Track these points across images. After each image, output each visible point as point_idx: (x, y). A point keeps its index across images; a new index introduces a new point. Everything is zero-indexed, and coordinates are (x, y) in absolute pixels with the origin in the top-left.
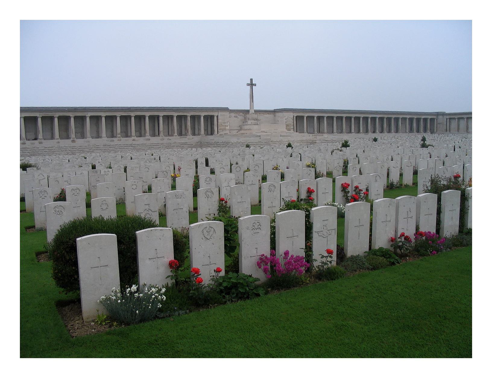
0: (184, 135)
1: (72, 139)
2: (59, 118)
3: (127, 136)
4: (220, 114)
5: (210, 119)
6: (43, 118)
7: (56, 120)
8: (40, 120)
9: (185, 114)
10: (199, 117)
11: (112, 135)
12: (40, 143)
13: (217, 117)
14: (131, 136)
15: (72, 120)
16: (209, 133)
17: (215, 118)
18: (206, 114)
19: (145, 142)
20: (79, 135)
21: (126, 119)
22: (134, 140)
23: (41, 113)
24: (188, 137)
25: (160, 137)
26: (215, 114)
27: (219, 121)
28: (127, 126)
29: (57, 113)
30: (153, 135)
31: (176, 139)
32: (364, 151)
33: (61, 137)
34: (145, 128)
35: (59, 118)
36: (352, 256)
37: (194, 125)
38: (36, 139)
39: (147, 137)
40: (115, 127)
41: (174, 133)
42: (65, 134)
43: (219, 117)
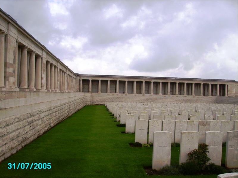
0: (206, 95)
1: (143, 94)
2: (137, 82)
3: (173, 94)
4: (229, 84)
5: (223, 87)
6: (128, 82)
7: (135, 83)
8: (127, 83)
9: (208, 83)
10: (116, 81)
11: (165, 93)
12: (126, 95)
13: (228, 85)
14: (175, 94)
15: (144, 83)
16: (222, 95)
17: (226, 86)
18: (221, 83)
19: (184, 98)
20: (146, 92)
21: (173, 84)
22: (177, 97)
23: (128, 79)
24: (209, 96)
25: (193, 96)
26: (226, 84)
27: (229, 88)
28: (165, 89)
29: (136, 79)
30: (188, 94)
31: (201, 97)
32: (223, 114)
33: (145, 93)
34: (191, 90)
35: (137, 82)
36: (136, 142)
37: (220, 92)
38: (124, 93)
39: (185, 96)
40: (158, 89)
41: (201, 94)
42: (189, 93)
43: (229, 86)
